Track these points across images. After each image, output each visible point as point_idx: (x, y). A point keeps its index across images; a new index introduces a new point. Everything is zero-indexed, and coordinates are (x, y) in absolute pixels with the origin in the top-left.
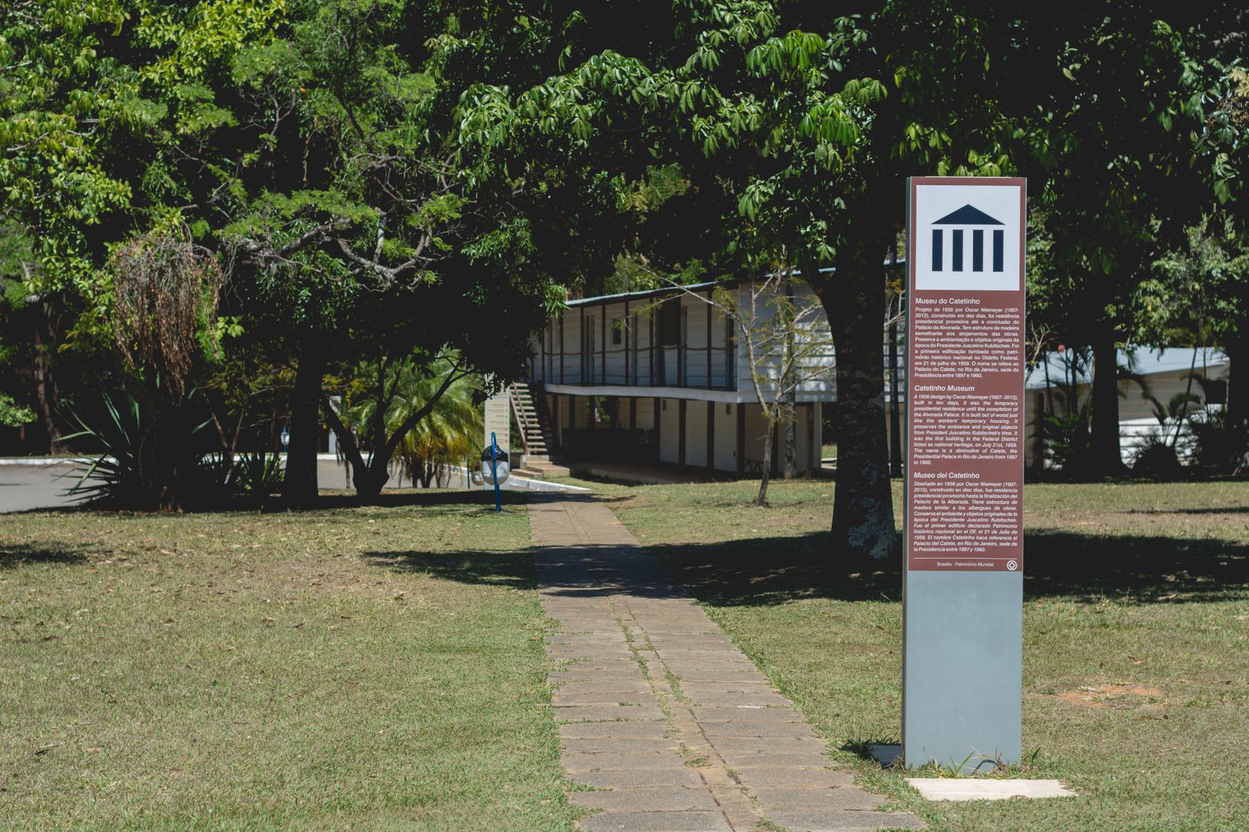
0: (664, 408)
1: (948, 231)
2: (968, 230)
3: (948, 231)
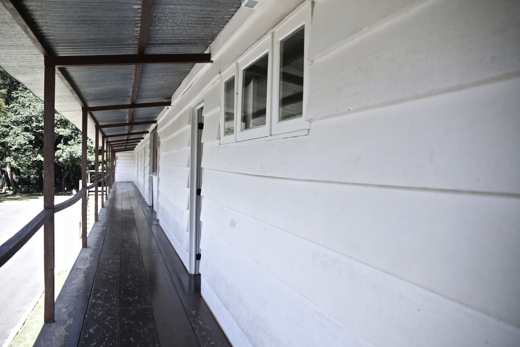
0: (80, 224)
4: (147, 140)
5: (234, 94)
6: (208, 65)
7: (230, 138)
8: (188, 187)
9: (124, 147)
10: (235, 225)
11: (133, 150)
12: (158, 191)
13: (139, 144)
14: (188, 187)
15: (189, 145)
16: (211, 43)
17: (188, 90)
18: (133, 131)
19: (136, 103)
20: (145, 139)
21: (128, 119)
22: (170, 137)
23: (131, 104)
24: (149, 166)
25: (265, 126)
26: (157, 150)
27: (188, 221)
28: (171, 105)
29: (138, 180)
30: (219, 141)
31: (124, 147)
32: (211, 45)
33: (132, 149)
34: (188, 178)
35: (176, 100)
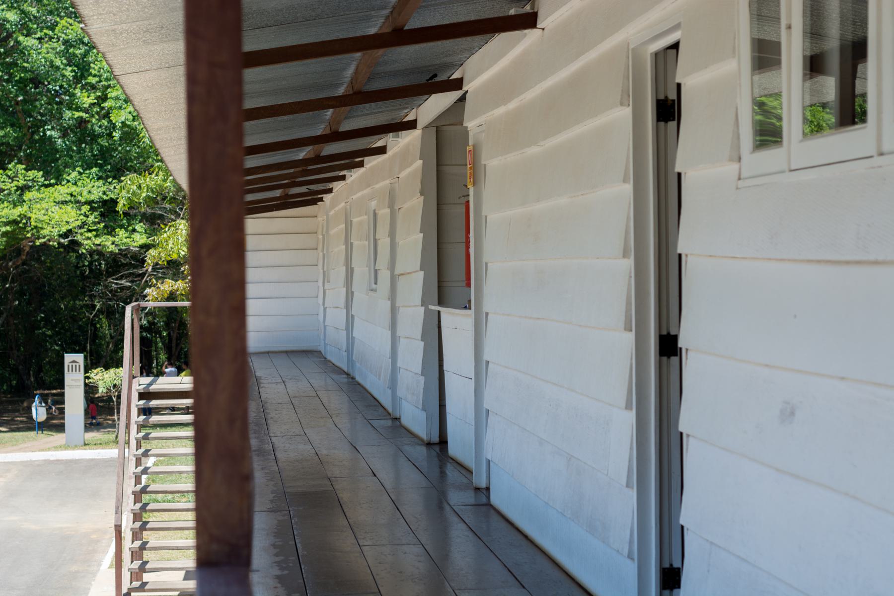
1: (70, 365)
2: (74, 364)
3: (70, 365)
4: (404, 159)
5: (780, 28)
7: (771, 157)
8: (628, 329)
9: (278, 193)
10: (792, 413)
11: (314, 202)
12: (480, 365)
13: (353, 176)
14: (628, 329)
15: (625, 181)
18: (346, 126)
19: (406, 28)
20: (390, 153)
21: (348, 80)
22: (533, 150)
23: (387, 30)
24: (421, 269)
25: (865, 128)
26: (468, 202)
27: (631, 448)
28: (538, 27)
29: (350, 340)
30: (735, 166)
31: (278, 193)
33: (313, 199)
34: (624, 298)
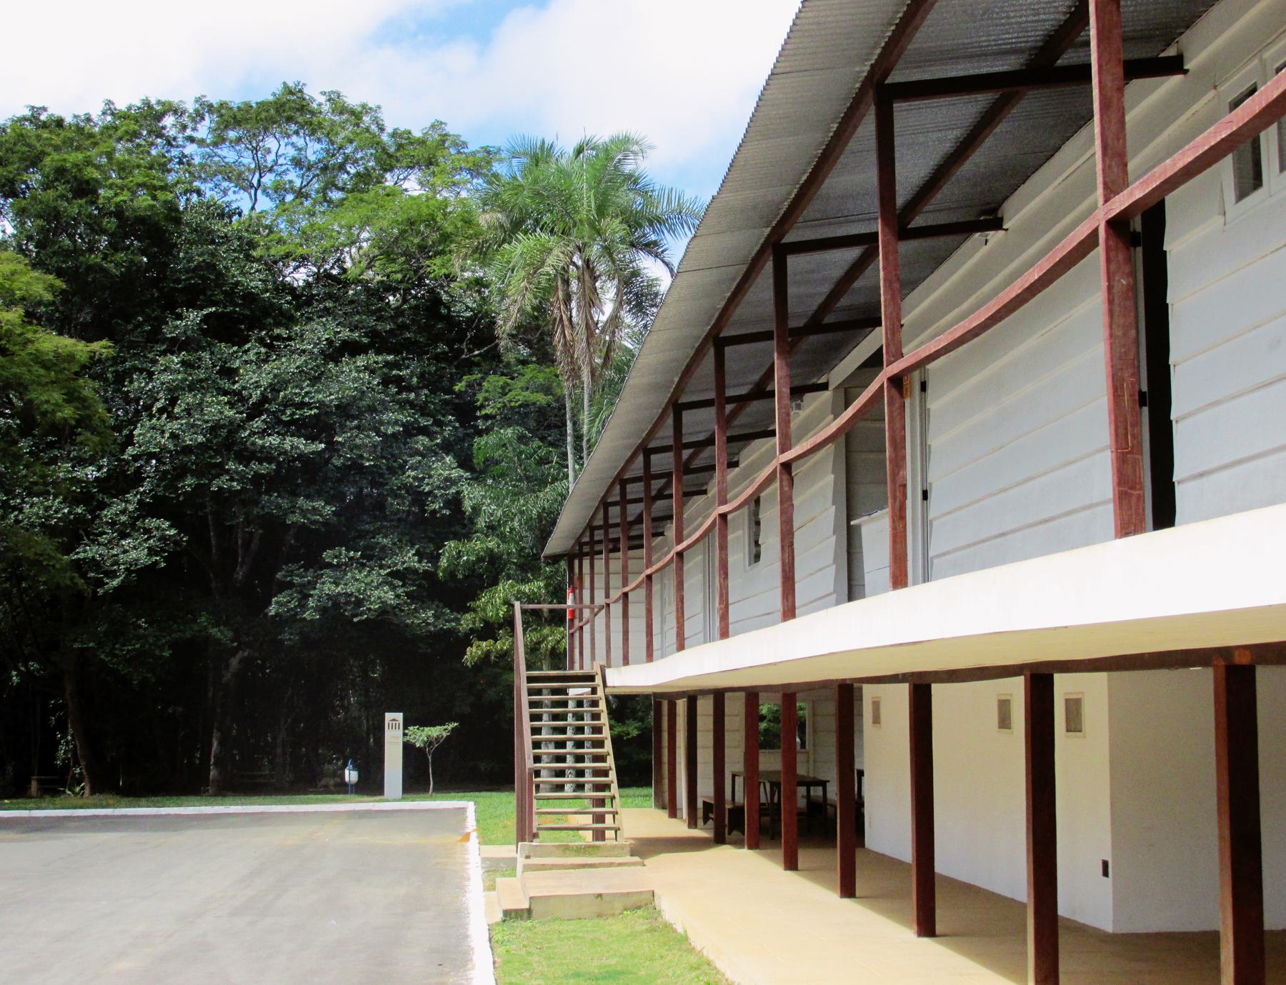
0: (877, 720)
2: (394, 722)
6: (1176, 79)
16: (1182, 33)
17: (1073, 176)
20: (742, 465)
32: (1183, 39)
35: (1018, 213)
